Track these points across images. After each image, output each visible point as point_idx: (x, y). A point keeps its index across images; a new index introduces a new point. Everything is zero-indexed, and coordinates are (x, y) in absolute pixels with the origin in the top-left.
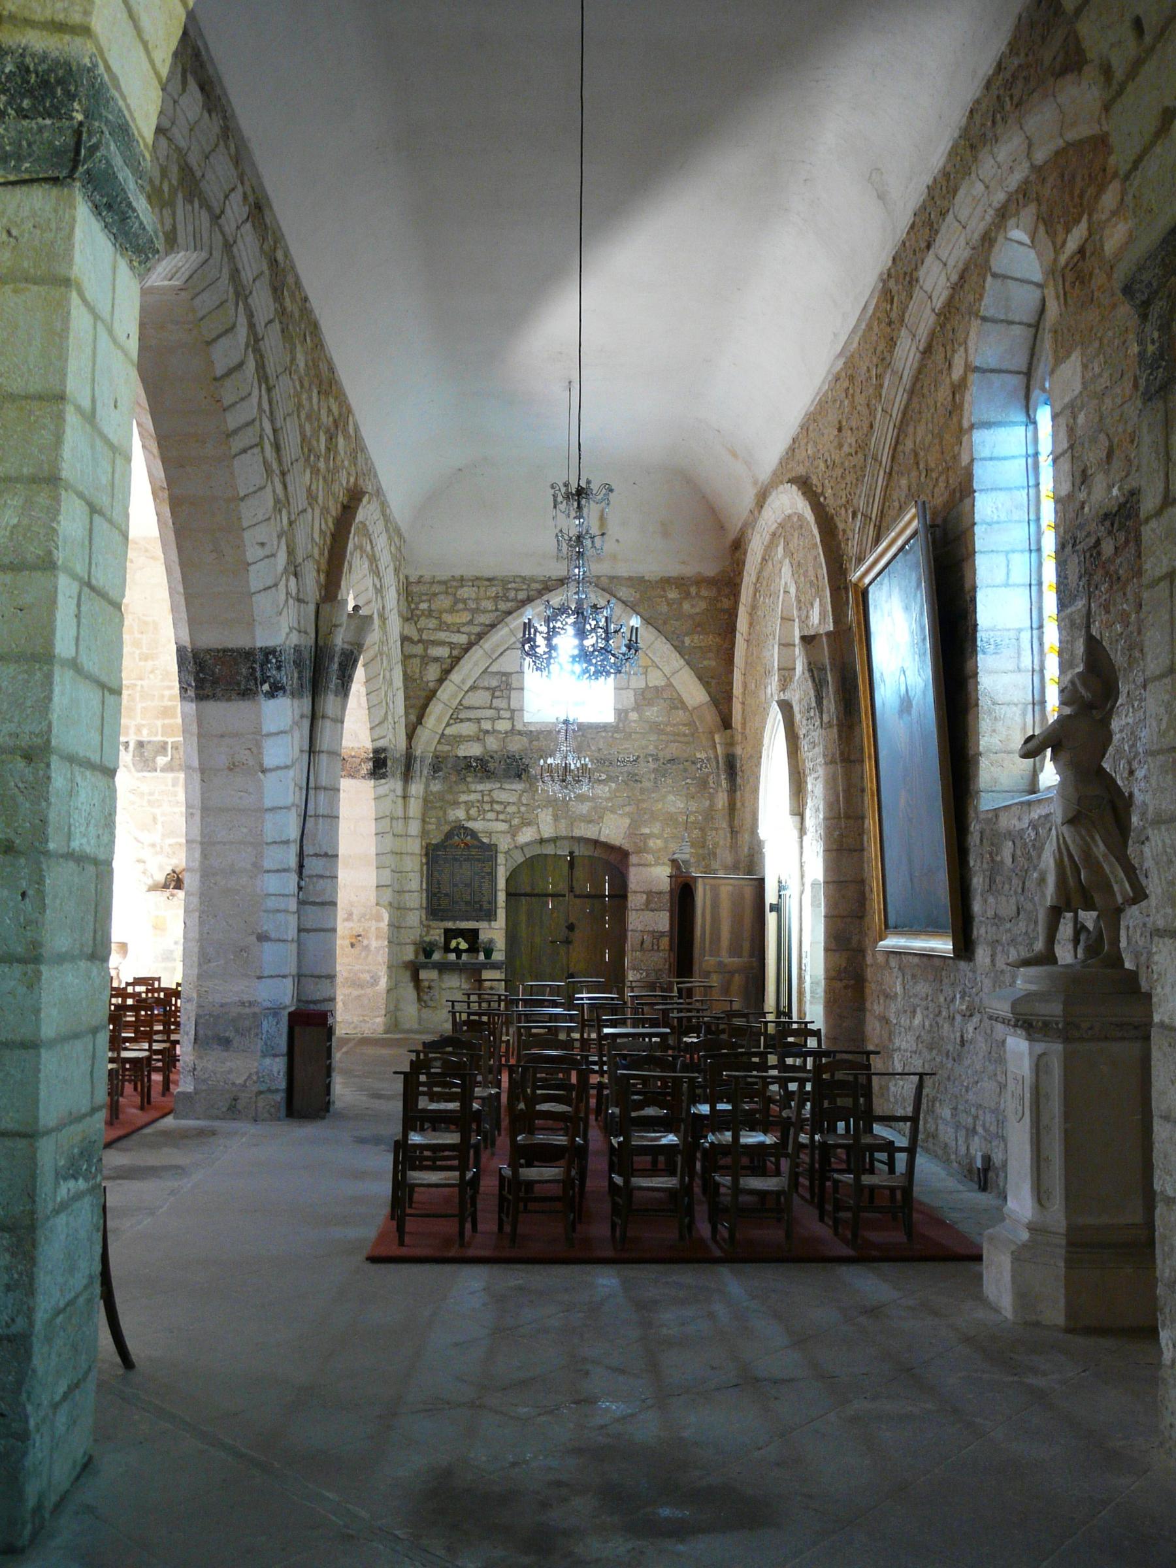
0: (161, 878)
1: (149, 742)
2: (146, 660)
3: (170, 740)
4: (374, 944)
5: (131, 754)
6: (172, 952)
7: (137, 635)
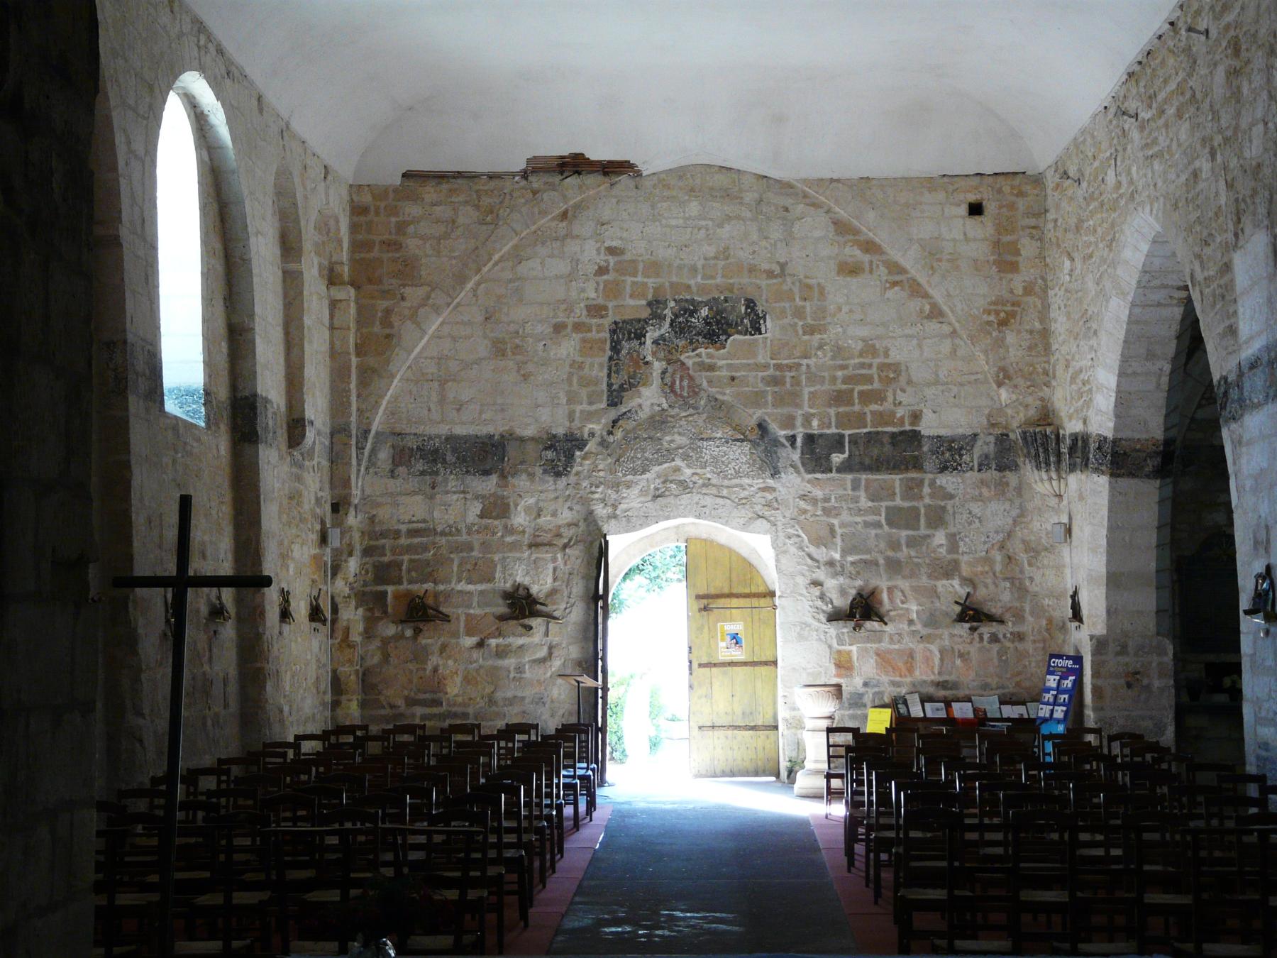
0: (842, 603)
1: (821, 435)
2: (812, 334)
3: (847, 432)
4: (1157, 683)
5: (799, 451)
6: (861, 696)
7: (799, 302)
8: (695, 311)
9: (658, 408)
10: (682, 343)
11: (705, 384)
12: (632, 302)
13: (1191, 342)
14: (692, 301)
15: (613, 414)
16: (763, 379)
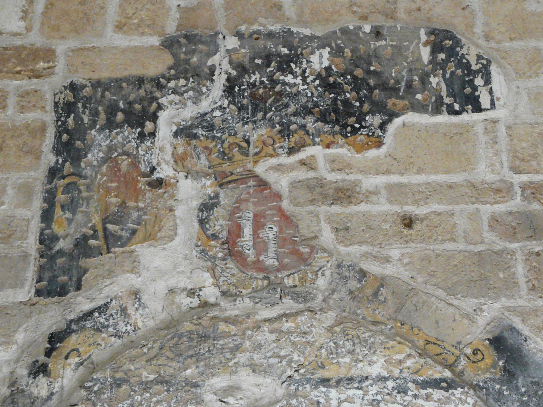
8: (295, 58)
9: (186, 301)
10: (259, 133)
11: (327, 236)
12: (121, 41)
13: (527, 237)
14: (287, 37)
15: (52, 316)
16: (495, 221)
